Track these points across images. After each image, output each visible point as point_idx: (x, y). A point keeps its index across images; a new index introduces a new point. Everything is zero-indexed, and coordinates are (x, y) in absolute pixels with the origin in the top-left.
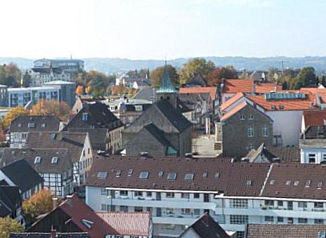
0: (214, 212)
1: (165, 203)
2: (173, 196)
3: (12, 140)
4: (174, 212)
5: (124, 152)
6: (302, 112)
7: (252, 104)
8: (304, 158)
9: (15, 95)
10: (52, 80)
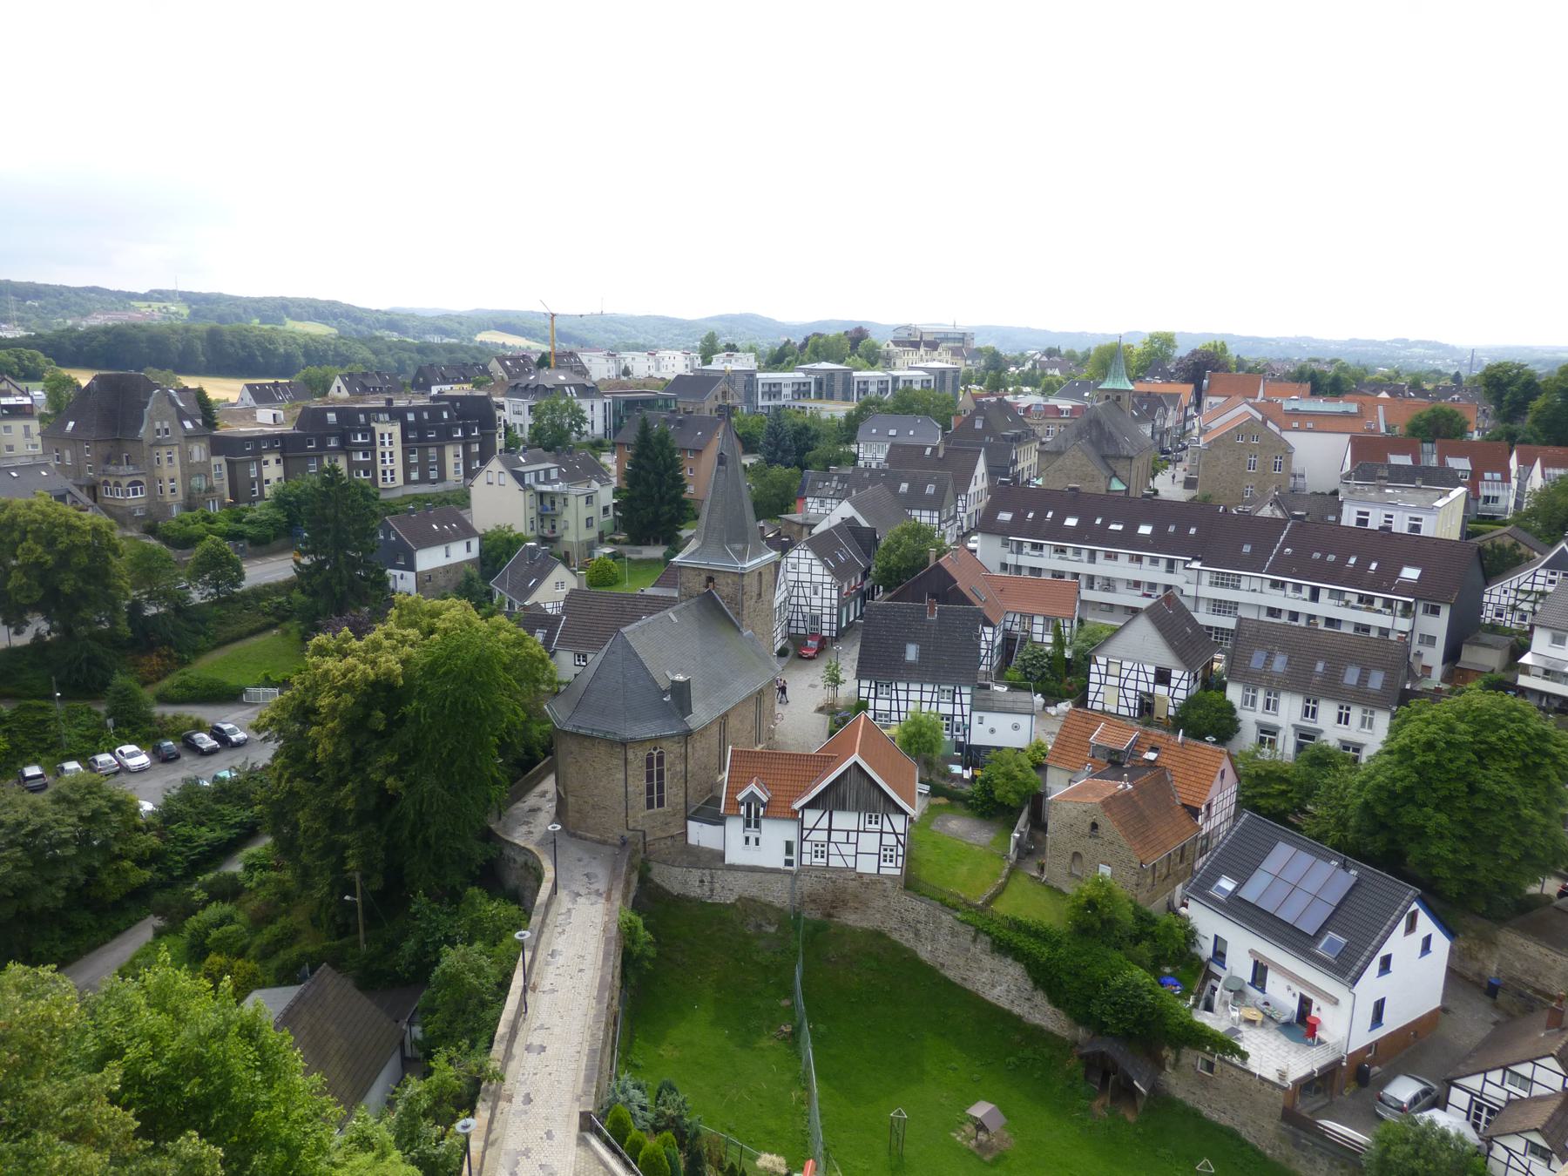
1: (1102, 568)
2: (1116, 558)
6: (1348, 437)
7: (1260, 417)
8: (1349, 518)
9: (865, 383)
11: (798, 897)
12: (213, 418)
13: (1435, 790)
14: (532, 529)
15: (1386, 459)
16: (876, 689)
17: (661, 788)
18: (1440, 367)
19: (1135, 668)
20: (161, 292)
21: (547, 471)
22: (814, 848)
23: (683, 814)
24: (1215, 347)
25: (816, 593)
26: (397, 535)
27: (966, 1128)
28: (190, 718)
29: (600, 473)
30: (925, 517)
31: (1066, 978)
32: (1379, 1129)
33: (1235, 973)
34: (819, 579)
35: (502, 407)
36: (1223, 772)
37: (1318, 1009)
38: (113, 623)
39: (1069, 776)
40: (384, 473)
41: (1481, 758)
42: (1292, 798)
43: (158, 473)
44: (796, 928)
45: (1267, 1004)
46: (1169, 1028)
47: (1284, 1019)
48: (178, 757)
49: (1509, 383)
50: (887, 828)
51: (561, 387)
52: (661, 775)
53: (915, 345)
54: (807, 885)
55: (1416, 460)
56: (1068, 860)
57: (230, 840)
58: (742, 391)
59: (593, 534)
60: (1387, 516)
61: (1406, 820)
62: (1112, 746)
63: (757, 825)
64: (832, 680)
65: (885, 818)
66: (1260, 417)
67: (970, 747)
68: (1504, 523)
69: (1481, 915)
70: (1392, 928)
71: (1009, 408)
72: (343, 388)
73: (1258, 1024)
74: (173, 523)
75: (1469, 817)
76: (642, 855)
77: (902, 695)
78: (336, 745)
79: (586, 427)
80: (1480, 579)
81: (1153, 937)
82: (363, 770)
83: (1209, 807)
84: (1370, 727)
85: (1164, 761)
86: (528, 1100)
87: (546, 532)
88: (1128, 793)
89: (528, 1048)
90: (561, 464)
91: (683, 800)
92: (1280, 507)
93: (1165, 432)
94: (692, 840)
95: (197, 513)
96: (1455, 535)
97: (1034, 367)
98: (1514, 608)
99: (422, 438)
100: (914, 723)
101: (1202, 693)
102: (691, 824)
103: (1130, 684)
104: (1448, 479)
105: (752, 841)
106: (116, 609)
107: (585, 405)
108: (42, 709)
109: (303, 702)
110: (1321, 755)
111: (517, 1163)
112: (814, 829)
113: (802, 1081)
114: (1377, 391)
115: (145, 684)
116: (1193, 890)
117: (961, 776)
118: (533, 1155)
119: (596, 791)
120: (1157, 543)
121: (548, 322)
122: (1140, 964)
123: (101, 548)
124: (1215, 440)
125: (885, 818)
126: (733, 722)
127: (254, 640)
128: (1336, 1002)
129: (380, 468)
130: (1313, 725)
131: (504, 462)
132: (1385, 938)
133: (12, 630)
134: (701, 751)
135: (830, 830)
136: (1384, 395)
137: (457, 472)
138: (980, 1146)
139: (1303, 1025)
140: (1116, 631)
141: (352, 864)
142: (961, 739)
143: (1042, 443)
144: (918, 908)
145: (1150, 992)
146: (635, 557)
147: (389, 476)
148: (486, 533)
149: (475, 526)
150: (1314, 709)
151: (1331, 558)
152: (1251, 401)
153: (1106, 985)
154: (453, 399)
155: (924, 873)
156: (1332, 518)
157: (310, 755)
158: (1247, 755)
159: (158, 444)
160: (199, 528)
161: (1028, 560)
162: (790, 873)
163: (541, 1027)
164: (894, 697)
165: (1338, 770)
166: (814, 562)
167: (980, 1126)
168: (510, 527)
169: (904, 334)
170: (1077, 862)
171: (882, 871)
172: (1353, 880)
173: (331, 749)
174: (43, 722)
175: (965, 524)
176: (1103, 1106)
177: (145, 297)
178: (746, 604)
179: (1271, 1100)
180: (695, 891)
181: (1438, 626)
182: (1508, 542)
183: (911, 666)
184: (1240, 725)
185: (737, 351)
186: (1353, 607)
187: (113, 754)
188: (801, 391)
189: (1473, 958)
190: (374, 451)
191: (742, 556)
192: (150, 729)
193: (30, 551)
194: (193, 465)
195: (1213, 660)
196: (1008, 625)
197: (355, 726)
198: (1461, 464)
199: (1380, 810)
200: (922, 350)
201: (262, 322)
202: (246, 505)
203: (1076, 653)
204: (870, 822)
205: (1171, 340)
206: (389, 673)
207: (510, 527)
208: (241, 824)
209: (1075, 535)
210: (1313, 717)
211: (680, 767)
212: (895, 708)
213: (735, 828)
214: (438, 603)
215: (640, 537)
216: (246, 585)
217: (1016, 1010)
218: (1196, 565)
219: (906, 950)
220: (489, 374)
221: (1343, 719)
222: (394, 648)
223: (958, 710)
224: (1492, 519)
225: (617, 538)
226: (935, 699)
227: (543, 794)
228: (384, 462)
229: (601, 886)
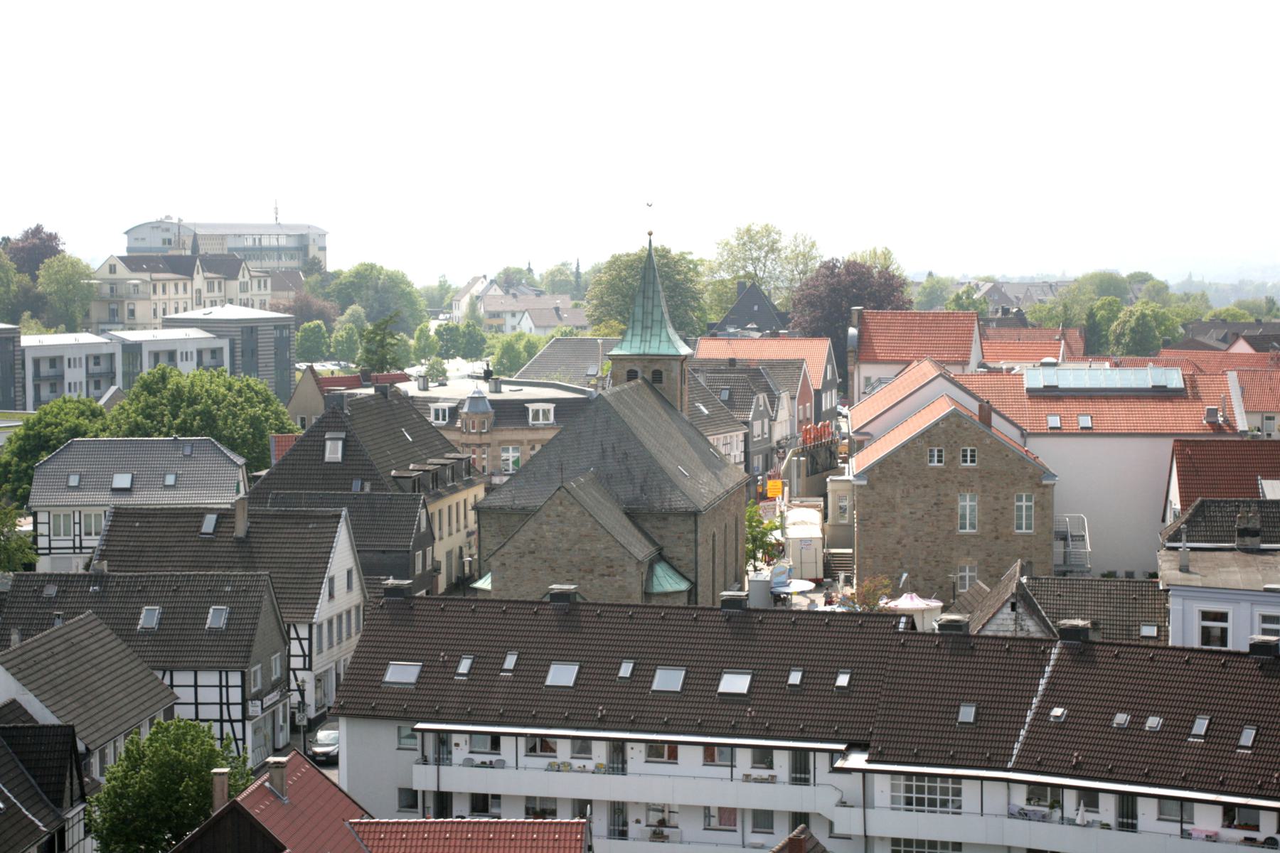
0: (831, 824)
2: (673, 756)
3: (42, 542)
4: (675, 819)
5: (485, 583)
6: (1168, 444)
9: (54, 362)
10: (200, 303)
15: (1256, 489)
53: (182, 267)
92: (1033, 611)
114: (1230, 339)
136: (1242, 347)
151: (1153, 722)
169: (154, 242)
175: (310, 698)
200: (199, 280)
218: (858, 760)
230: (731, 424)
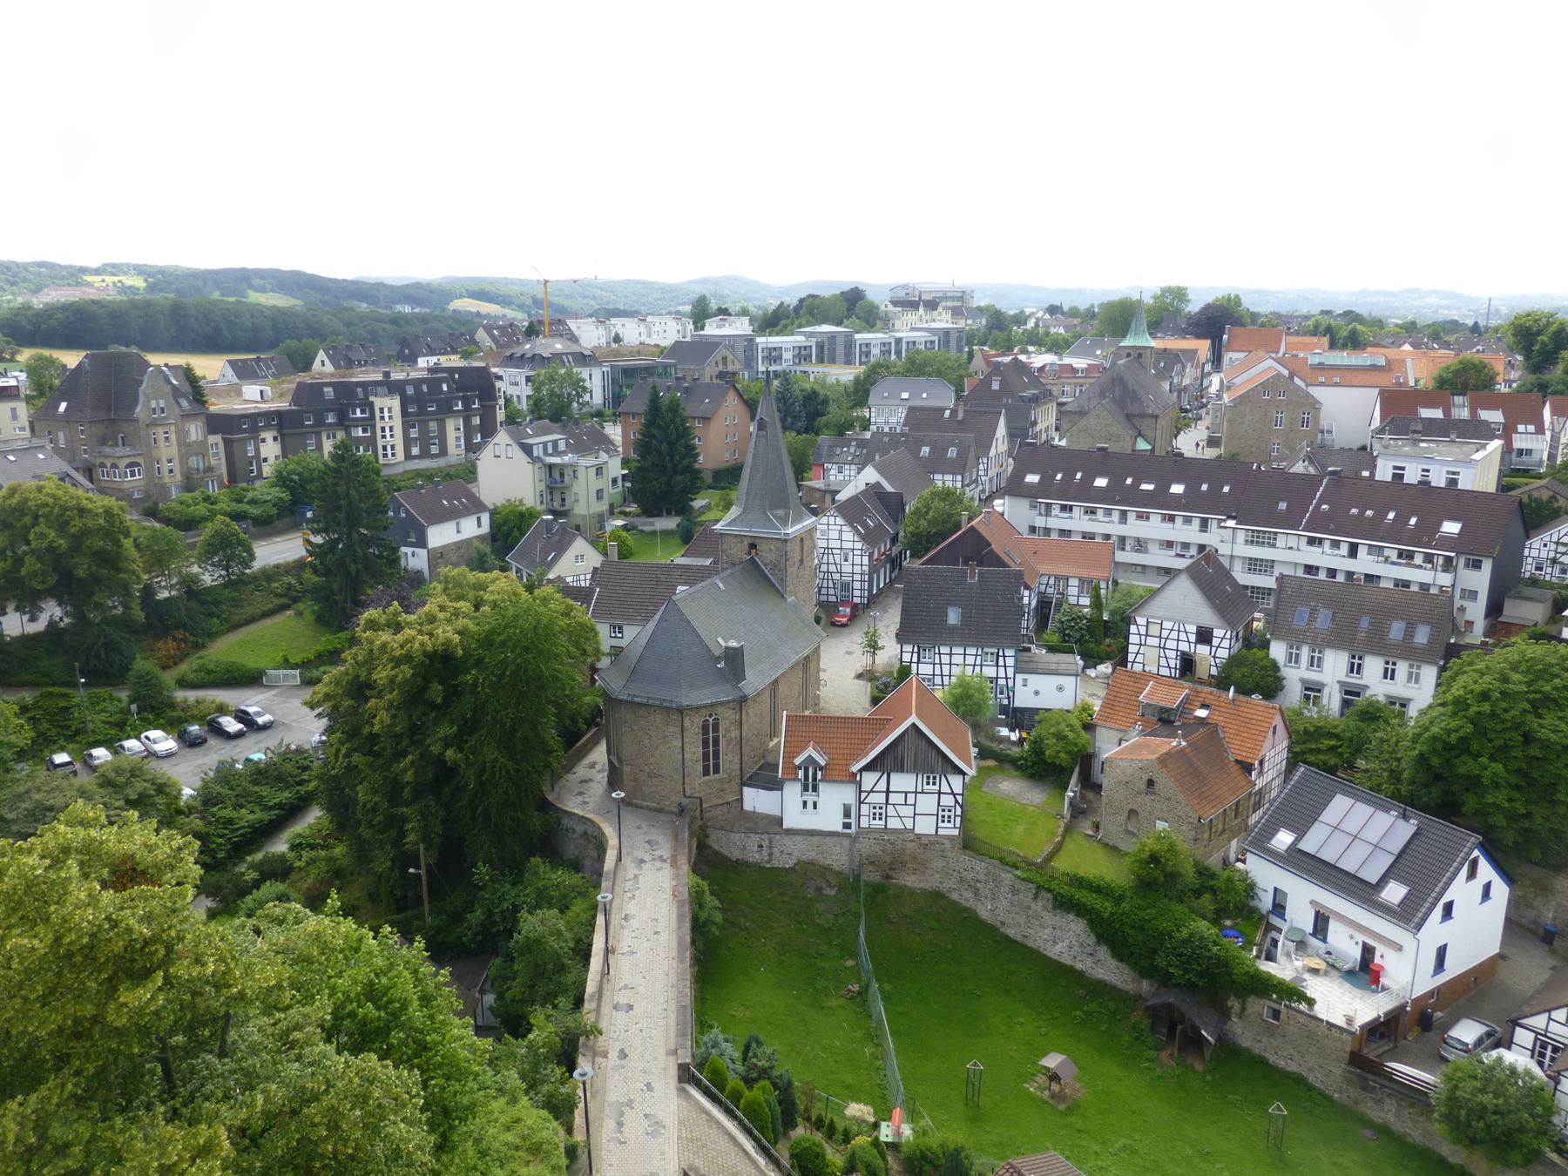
1: (1134, 528)
2: (1148, 518)
8: (1384, 472)
9: (867, 345)
11: (857, 859)
12: (202, 396)
13: (1490, 740)
14: (542, 503)
15: (1416, 413)
16: (919, 653)
17: (716, 755)
18: (1456, 318)
19: (1176, 628)
20: (114, 266)
21: (555, 443)
22: (872, 811)
23: (738, 780)
24: (1229, 299)
25: (846, 560)
26: (407, 512)
27: (1038, 1079)
28: (213, 702)
29: (606, 442)
30: (946, 481)
31: (1131, 932)
32: (1447, 1069)
33: (1296, 925)
34: (850, 545)
35: (500, 378)
36: (1275, 727)
37: (1382, 956)
38: (127, 607)
39: (1120, 735)
40: (385, 448)
41: (1535, 708)
42: (1342, 754)
43: (155, 453)
44: (856, 890)
45: (1329, 953)
46: (1235, 977)
47: (1347, 967)
48: (205, 741)
49: (1539, 333)
50: (945, 788)
51: (557, 356)
52: (716, 741)
53: (913, 305)
54: (866, 847)
55: (1447, 413)
56: (1124, 817)
57: (271, 821)
58: (742, 356)
59: (603, 507)
60: (1424, 470)
61: (1462, 770)
62: (1163, 704)
63: (815, 789)
64: (870, 646)
65: (943, 778)
66: (1286, 373)
67: (1016, 710)
68: (1539, 476)
69: (1536, 864)
70: (1455, 875)
71: (1022, 368)
72: (327, 362)
73: (1322, 972)
74: (173, 505)
75: (1524, 766)
76: (700, 823)
77: (945, 659)
78: (394, 717)
79: (587, 397)
80: (1520, 531)
81: (1214, 891)
82: (421, 742)
83: (1261, 763)
84: (1417, 681)
85: (1218, 719)
86: (623, 1055)
87: (556, 505)
88: (1183, 749)
89: (616, 1007)
90: (570, 435)
91: (738, 766)
93: (1182, 390)
94: (748, 806)
95: (197, 494)
96: (1492, 488)
97: (1037, 325)
98: (1554, 561)
99: (422, 411)
100: (960, 686)
101: (1244, 651)
102: (746, 790)
103: (1171, 644)
104: (1482, 432)
105: (810, 805)
106: (128, 594)
107: (584, 373)
108: (64, 696)
109: (358, 676)
110: (1371, 709)
111: (622, 1114)
112: (872, 791)
113: (874, 1038)
115: (164, 668)
116: (1251, 843)
117: (1008, 738)
118: (637, 1105)
119: (651, 760)
120: (1189, 502)
121: (542, 286)
122: (1204, 917)
123: (113, 529)
124: (1240, 396)
125: (943, 778)
126: (782, 688)
127: (268, 622)
128: (1400, 948)
129: (380, 443)
130: (1358, 682)
131: (512, 435)
132: (1448, 885)
133: (26, 618)
134: (755, 716)
135: (888, 792)
137: (458, 446)
138: (1053, 1096)
139: (1366, 972)
140: (1154, 593)
141: (411, 838)
142: (1005, 702)
143: (1060, 405)
144: (978, 867)
145: (1215, 944)
146: (647, 528)
147: (389, 451)
148: (496, 508)
149: (483, 498)
150: (1359, 665)
151: (1369, 513)
152: (1274, 355)
153: (1171, 937)
154: (451, 371)
155: (980, 833)
156: (1366, 474)
157: (366, 730)
158: (1294, 711)
159: (154, 423)
160: (201, 509)
161: (1057, 521)
162: (849, 835)
163: (626, 987)
164: (937, 661)
165: (1389, 724)
166: (844, 528)
167: (1054, 1077)
168: (521, 501)
169: (901, 294)
170: (1133, 819)
171: (941, 832)
172: (1414, 829)
173: (388, 721)
174: (66, 709)
176: (1171, 1056)
177: (97, 272)
178: (789, 570)
179: (1339, 1045)
180: (754, 856)
181: (1480, 580)
182: (1545, 495)
183: (953, 630)
184: (1285, 682)
185: (730, 315)
186: (1393, 563)
187: (139, 739)
188: (802, 355)
189: (1529, 906)
190: (374, 427)
191: (784, 521)
192: (175, 714)
193: (43, 535)
194: (190, 445)
195: (1253, 619)
196: (1043, 588)
197: (414, 697)
198: (1495, 416)
199: (1435, 761)
200: (921, 310)
201: (223, 295)
202: (244, 485)
203: (1113, 613)
204: (928, 783)
205: (1184, 295)
206: (448, 642)
207: (521, 501)
208: (280, 806)
209: (1105, 496)
210: (1358, 673)
211: (735, 734)
212: (938, 672)
213: (792, 792)
214: (482, 576)
215: (652, 508)
216: (257, 565)
217: (1079, 966)
218: (1231, 523)
219: (966, 910)
220: (477, 344)
221: (1389, 674)
222: (449, 621)
223: (1002, 673)
224: (1526, 472)
225: (628, 510)
226: (978, 662)
227: (592, 766)
228: (384, 437)
229: (665, 852)
230: (1165, 378)
